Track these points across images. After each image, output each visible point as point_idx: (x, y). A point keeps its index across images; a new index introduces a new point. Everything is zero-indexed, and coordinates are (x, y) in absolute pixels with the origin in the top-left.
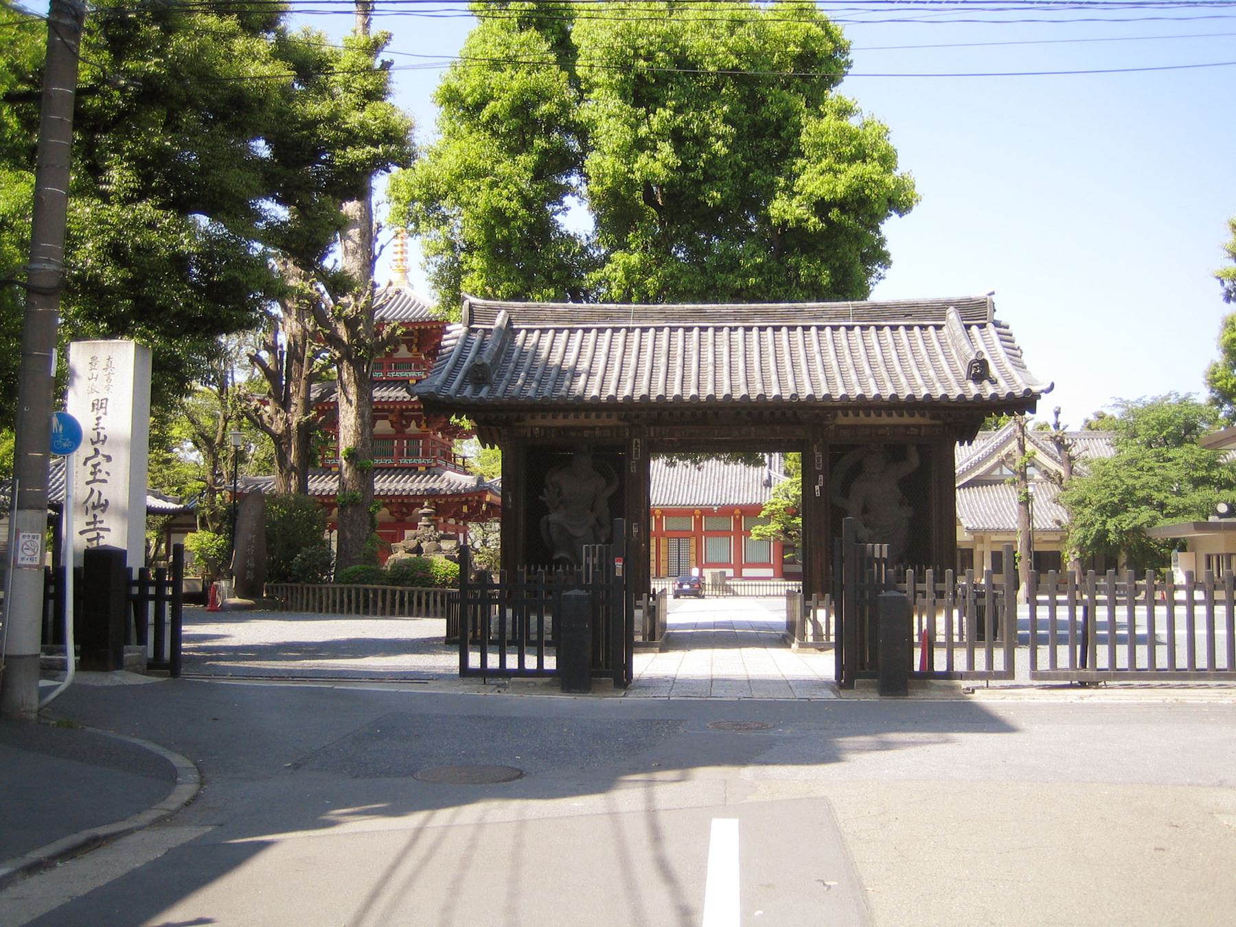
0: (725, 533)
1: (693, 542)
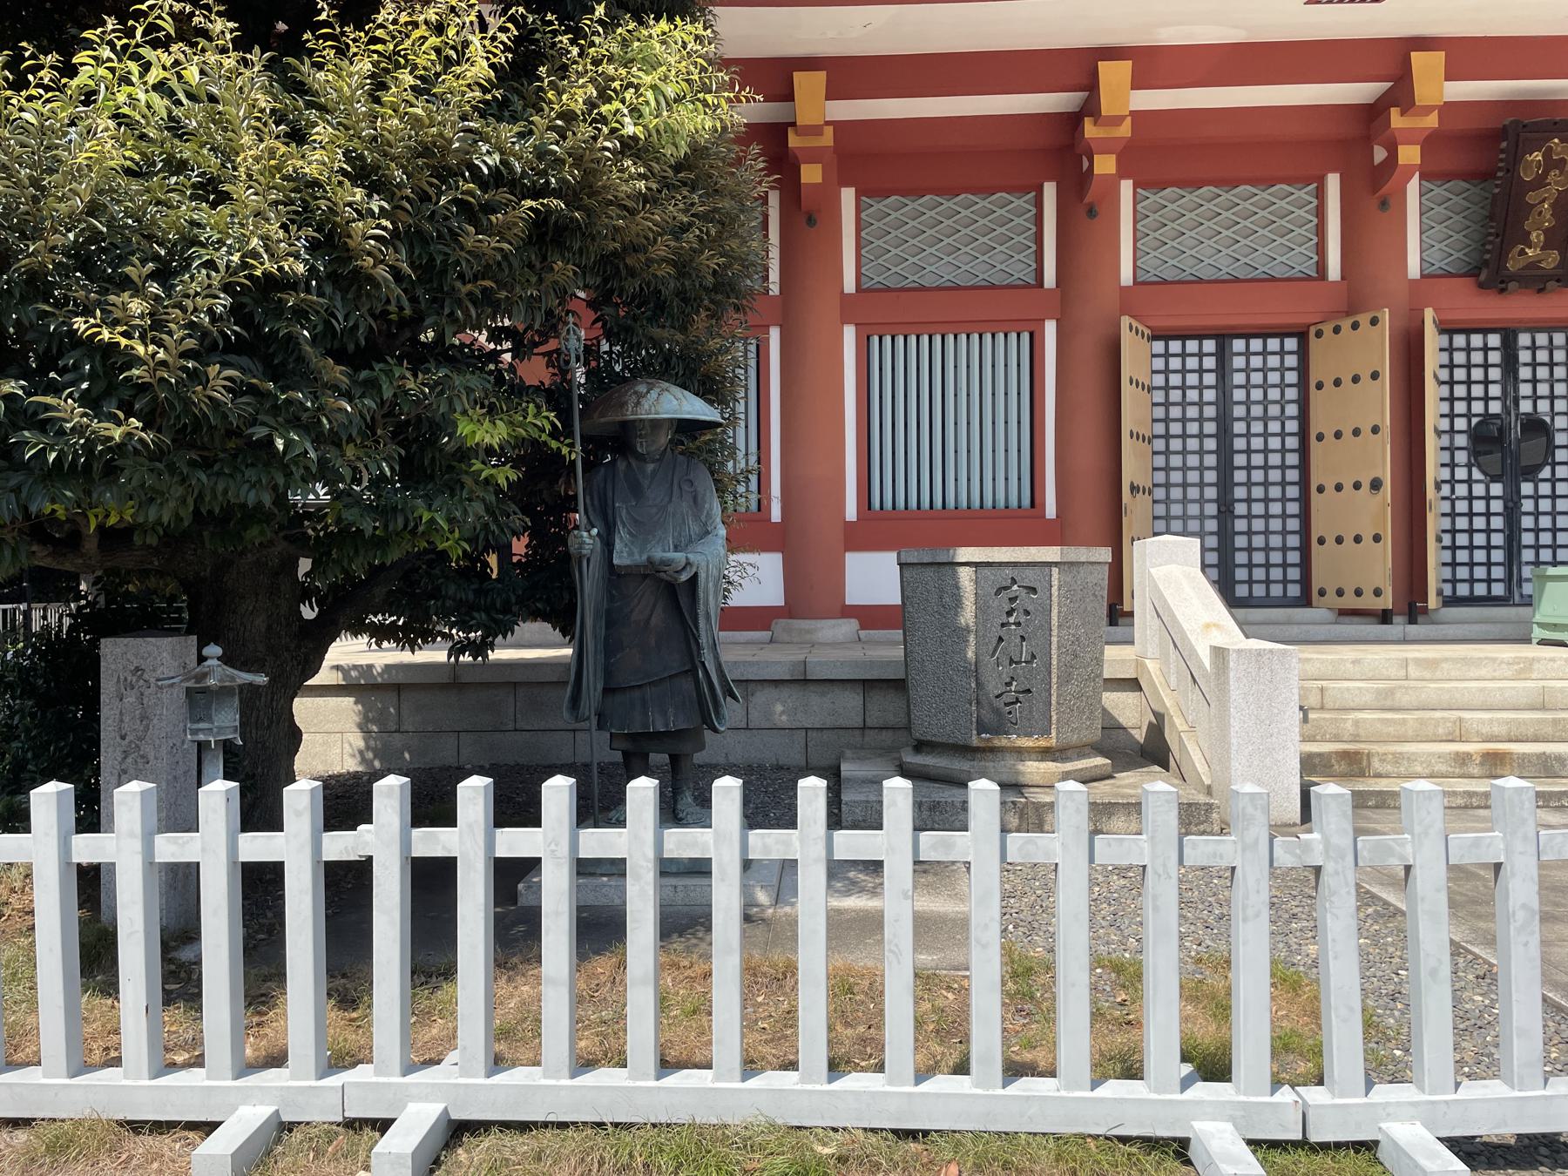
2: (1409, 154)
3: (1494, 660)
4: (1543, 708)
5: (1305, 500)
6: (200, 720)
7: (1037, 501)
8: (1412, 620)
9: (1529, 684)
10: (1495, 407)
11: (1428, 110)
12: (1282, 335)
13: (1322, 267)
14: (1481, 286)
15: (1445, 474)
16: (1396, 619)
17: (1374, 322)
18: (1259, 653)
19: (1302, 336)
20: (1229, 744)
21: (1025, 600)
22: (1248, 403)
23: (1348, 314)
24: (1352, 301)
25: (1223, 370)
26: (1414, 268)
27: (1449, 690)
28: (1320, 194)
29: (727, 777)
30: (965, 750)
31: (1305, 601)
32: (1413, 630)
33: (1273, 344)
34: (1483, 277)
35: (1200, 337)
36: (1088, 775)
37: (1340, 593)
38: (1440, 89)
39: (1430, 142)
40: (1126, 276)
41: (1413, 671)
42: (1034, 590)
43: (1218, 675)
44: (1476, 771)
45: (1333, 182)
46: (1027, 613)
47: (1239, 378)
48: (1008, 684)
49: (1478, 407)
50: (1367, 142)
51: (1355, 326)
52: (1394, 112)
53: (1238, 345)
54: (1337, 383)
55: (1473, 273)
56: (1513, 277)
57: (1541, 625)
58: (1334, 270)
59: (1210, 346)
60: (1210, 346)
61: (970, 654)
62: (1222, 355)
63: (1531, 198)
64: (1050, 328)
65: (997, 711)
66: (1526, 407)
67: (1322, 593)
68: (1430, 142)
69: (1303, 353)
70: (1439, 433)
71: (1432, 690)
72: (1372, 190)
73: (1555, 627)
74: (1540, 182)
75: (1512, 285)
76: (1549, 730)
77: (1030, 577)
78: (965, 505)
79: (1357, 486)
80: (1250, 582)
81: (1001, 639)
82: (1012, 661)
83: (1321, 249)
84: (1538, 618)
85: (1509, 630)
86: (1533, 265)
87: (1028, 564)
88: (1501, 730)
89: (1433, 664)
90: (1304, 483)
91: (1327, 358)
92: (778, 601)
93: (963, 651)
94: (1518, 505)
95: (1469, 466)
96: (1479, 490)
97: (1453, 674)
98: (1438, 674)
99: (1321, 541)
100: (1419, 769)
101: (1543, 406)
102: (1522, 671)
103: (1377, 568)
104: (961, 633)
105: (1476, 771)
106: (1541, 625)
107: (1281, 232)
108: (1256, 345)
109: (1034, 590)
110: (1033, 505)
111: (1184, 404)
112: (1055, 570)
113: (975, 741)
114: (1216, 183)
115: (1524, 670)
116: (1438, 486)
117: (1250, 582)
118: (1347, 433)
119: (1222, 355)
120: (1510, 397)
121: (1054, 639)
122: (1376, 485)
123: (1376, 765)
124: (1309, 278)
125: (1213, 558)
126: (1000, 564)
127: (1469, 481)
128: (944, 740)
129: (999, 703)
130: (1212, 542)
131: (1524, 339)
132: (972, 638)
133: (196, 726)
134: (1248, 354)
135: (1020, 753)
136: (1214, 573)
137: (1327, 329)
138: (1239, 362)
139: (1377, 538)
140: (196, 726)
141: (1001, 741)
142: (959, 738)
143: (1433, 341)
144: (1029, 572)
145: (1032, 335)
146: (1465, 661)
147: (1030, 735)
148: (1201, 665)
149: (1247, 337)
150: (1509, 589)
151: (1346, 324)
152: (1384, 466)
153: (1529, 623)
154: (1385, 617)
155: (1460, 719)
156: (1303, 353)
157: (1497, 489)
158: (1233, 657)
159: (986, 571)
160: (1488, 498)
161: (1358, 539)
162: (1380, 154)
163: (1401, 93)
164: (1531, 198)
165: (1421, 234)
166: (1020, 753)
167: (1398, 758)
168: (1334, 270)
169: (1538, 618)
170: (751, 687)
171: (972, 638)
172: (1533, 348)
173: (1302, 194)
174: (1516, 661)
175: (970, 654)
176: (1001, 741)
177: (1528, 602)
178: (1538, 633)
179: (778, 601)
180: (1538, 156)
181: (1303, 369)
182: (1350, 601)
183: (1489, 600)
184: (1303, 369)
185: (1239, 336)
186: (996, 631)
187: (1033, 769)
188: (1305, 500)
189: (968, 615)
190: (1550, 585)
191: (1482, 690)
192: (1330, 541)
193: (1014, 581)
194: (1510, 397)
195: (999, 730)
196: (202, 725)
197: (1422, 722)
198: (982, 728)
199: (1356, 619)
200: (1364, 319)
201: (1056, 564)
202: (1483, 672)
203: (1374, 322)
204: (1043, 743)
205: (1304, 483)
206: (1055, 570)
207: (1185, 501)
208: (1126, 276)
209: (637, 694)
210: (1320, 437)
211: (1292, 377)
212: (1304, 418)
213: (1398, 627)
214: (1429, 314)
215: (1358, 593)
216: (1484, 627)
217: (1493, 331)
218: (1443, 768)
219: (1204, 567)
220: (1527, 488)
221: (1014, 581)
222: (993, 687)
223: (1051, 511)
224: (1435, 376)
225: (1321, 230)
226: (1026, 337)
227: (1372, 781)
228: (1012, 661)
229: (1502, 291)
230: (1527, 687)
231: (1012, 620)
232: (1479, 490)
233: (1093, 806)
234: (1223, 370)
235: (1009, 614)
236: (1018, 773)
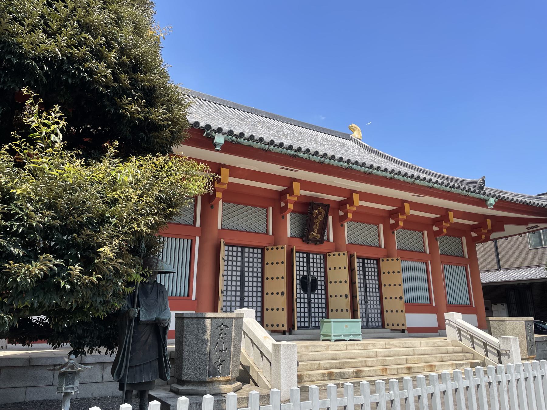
2: (291, 206)
3: (321, 345)
4: (334, 359)
5: (262, 297)
6: (70, 384)
7: (190, 294)
8: (290, 334)
9: (330, 352)
10: (305, 273)
11: (296, 196)
12: (258, 248)
13: (195, 222)
14: (303, 241)
15: (225, 288)
16: (287, 333)
17: (282, 248)
18: (288, 345)
19: (263, 249)
20: (281, 374)
21: (226, 330)
22: (249, 267)
23: (274, 245)
24: (275, 242)
25: (242, 257)
26: (289, 235)
27: (314, 355)
28: (267, 211)
29: (126, 404)
30: (203, 383)
31: (383, 327)
32: (291, 337)
33: (235, 249)
34: (304, 239)
35: (237, 247)
36: (235, 389)
37: (272, 325)
38: (298, 191)
39: (295, 204)
40: (219, 227)
41: (304, 350)
42: (227, 327)
43: (275, 353)
44: (326, 378)
45: (271, 209)
46: (225, 334)
47: (247, 260)
48: (219, 359)
49: (302, 273)
50: (280, 200)
51: (277, 248)
52: (288, 195)
53: (247, 250)
54: (277, 263)
55: (301, 237)
56: (311, 240)
57: (323, 335)
58: (271, 233)
59: (239, 249)
60: (239, 249)
61: (208, 349)
62: (243, 252)
63: (315, 221)
64: (197, 239)
65: (215, 368)
66: (312, 274)
67: (388, 325)
68: (295, 204)
69: (263, 254)
70: (223, 276)
71: (311, 355)
72: (280, 212)
73: (327, 336)
74: (317, 217)
75: (318, 243)
76: (338, 365)
77: (227, 323)
78: (175, 295)
79: (278, 294)
80: (305, 322)
81: (217, 343)
82: (220, 351)
83: (267, 226)
84: (322, 333)
85: (312, 336)
86: (315, 238)
87: (227, 318)
88: (328, 366)
89: (307, 347)
90: (262, 292)
91: (269, 256)
92: (436, 325)
93: (206, 348)
94: (311, 301)
95: (300, 289)
96: (302, 296)
97: (313, 350)
98: (309, 350)
99: (267, 310)
100: (314, 379)
101: (315, 274)
102: (326, 349)
104: (205, 342)
105: (326, 378)
106: (323, 335)
107: (256, 221)
108: (251, 250)
109: (227, 327)
110: (188, 295)
111: (232, 266)
112: (234, 320)
113: (207, 379)
114: (234, 203)
115: (327, 348)
116: (222, 292)
117: (305, 322)
118: (275, 278)
119: (243, 252)
120: (308, 271)
121: (232, 343)
122: (283, 294)
123: (305, 379)
124: (191, 225)
125: (259, 314)
126: (219, 318)
127: (318, 294)
128: (195, 380)
129: (215, 365)
130: (259, 309)
131: (247, 250)
132: (209, 343)
133: (67, 387)
134: (237, 252)
135: (220, 382)
136: (259, 319)
137: (270, 248)
138: (247, 255)
139: (283, 309)
140: (67, 387)
141: (215, 379)
142: (202, 379)
143: (223, 248)
144: (227, 321)
145: (192, 240)
146: (315, 346)
147: (223, 376)
148: (267, 349)
149: (249, 248)
150: (309, 324)
151: (275, 248)
152: (348, 292)
153: (319, 334)
154: (284, 333)
155: (320, 363)
156: (263, 254)
157: (306, 296)
158: (282, 347)
159: (215, 320)
160: (304, 298)
161: (278, 309)
162: (283, 204)
163: (290, 190)
164: (315, 221)
165: (290, 227)
166: (220, 382)
167: (310, 375)
168: (271, 233)
169: (322, 333)
170: (105, 365)
171: (209, 343)
172: (313, 258)
173: (263, 211)
174: (326, 346)
175: (208, 349)
176: (215, 379)
177: (319, 328)
178: (322, 337)
179: (436, 325)
180: (316, 211)
181: (263, 258)
182: (395, 327)
183: (377, 327)
184: (263, 258)
185: (247, 247)
186: (216, 340)
187: (224, 387)
188: (262, 297)
189: (208, 336)
190: (325, 324)
191: (321, 354)
192: (334, 311)
193: (222, 324)
194: (308, 271)
195: (215, 375)
196: (69, 386)
197: (311, 364)
198: (210, 374)
199: (276, 334)
200: (280, 247)
201: (234, 318)
202: (318, 349)
203: (282, 248)
204: (227, 378)
205: (262, 292)
206: (234, 320)
207: (231, 296)
208: (219, 227)
209: (138, 368)
210: (267, 279)
211: (260, 260)
212: (263, 272)
213: (287, 336)
214: (222, 240)
215: (278, 325)
216: (308, 336)
217: (305, 253)
218: (319, 378)
219: (257, 317)
220: (312, 296)
221: (222, 324)
222: (214, 360)
223: (194, 298)
224: (223, 259)
225: (267, 221)
226: (190, 241)
227: (305, 383)
228: (220, 351)
229: (308, 243)
230: (329, 354)
231: (221, 337)
232: (302, 296)
233: (239, 399)
234: (242, 257)
235: (220, 335)
236: (220, 389)
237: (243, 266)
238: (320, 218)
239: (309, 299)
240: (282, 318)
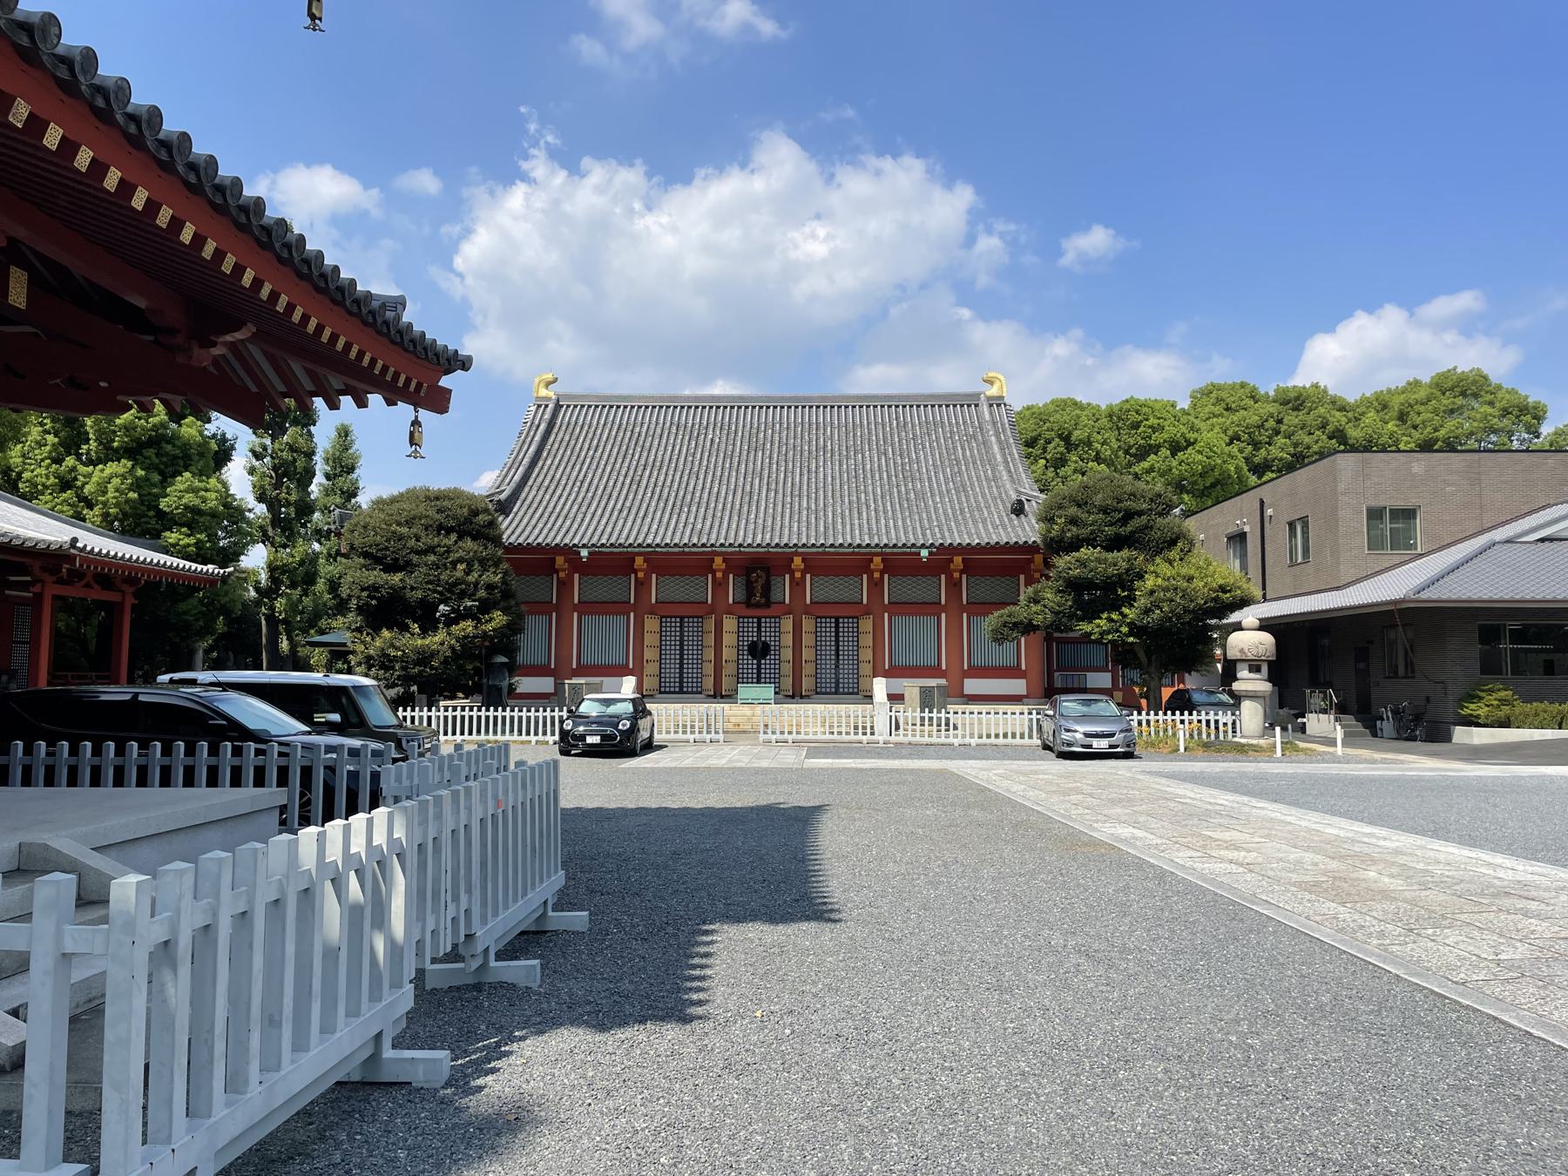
0: (618, 607)
1: (710, 624)
62: (682, 622)
103: (709, 683)
119: (682, 622)
120: (759, 636)
194: (759, 636)
237: (682, 636)
238: (761, 581)
239: (759, 665)
240: (787, 683)
